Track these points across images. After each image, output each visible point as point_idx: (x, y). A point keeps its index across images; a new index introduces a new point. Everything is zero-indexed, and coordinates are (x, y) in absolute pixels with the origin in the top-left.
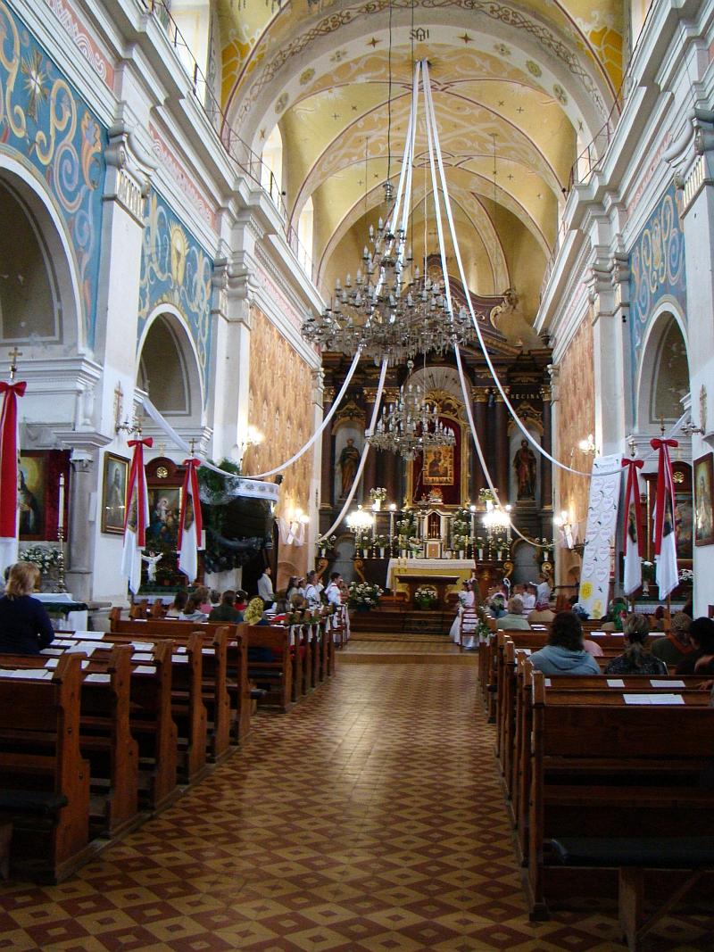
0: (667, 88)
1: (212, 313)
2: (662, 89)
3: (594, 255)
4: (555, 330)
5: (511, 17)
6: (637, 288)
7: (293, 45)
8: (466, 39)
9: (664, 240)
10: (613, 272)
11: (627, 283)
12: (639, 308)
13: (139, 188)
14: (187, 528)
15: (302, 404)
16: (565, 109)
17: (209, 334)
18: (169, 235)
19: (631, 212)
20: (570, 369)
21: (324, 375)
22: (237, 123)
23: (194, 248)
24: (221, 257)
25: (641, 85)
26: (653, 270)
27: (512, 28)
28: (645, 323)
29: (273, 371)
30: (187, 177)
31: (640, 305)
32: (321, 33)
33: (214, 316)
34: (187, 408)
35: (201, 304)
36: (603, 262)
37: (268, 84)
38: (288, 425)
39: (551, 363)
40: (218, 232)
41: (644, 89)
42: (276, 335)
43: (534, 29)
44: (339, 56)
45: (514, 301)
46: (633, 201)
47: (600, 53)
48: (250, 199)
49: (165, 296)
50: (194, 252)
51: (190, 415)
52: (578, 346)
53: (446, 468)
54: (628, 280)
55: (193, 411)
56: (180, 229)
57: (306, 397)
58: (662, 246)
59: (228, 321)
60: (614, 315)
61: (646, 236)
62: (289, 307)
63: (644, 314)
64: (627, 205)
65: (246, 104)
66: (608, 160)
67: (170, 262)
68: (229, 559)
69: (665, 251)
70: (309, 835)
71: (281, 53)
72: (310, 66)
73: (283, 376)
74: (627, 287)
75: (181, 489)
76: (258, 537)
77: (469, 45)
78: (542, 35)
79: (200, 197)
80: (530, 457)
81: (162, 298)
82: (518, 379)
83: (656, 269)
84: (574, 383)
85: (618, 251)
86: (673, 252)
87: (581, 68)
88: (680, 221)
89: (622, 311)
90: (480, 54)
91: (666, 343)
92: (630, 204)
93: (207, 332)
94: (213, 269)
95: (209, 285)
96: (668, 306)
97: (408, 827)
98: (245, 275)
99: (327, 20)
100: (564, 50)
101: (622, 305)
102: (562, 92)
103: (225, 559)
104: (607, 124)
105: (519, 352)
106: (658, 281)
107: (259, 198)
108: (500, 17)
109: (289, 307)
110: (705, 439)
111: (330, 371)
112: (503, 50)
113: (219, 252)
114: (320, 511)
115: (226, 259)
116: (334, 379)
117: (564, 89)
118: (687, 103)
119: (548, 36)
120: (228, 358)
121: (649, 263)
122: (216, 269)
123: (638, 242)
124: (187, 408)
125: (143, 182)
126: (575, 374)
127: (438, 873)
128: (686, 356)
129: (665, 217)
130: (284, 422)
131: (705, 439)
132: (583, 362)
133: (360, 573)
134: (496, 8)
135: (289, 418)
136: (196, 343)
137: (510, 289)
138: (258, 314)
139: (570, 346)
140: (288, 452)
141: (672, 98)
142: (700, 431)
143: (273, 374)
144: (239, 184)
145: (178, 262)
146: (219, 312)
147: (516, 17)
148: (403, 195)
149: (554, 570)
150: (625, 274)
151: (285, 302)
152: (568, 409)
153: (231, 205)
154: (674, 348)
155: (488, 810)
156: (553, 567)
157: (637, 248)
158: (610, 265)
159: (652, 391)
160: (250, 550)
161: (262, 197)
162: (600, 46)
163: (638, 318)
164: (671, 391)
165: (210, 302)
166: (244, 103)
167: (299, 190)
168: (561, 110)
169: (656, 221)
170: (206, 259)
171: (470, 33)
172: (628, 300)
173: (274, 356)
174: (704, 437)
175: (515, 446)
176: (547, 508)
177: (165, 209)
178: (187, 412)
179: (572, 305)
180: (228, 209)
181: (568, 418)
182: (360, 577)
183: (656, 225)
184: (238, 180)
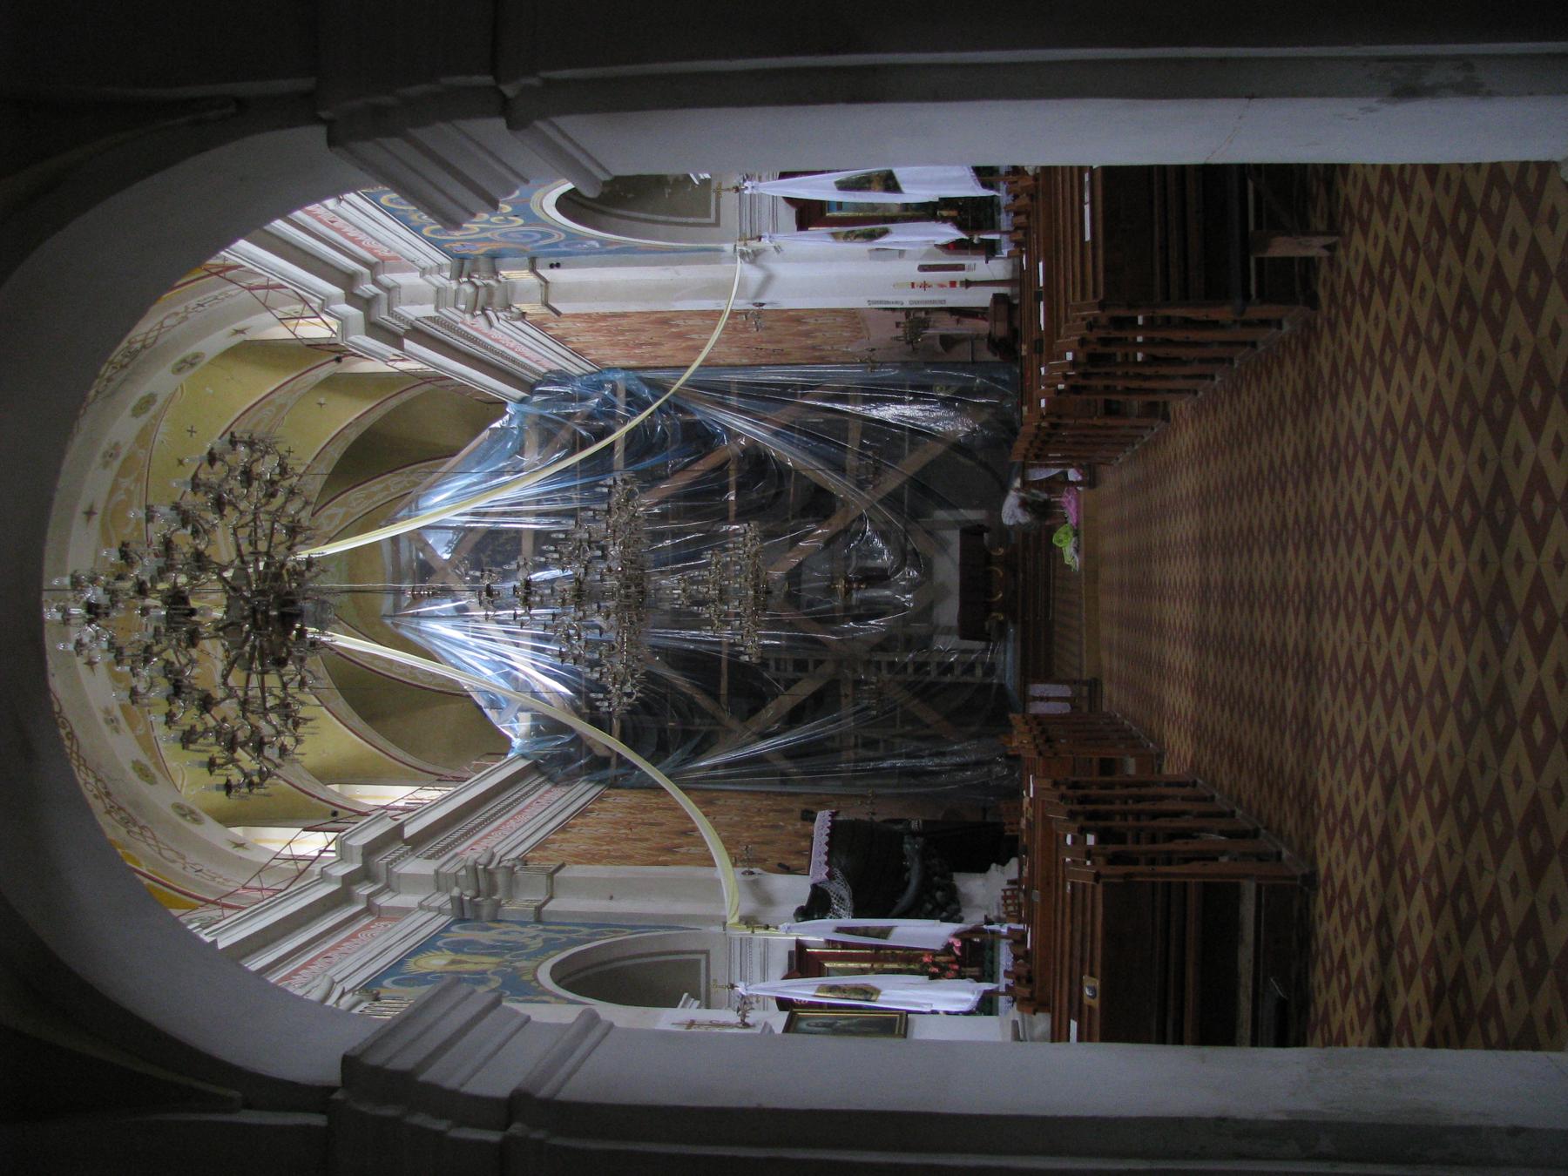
1: (539, 920)
3: (448, 312)
7: (95, 792)
8: (90, 513)
10: (478, 283)
11: (497, 262)
13: (365, 1004)
16: (209, 356)
18: (429, 974)
19: (385, 252)
22: (223, 884)
23: (439, 943)
24: (449, 906)
28: (565, 232)
30: (327, 951)
33: (545, 918)
35: (531, 936)
36: (462, 298)
37: (157, 834)
40: (406, 911)
42: (562, 836)
44: (111, 721)
46: (370, 250)
48: (352, 862)
49: (525, 978)
51: (707, 953)
52: (582, 339)
54: (494, 257)
55: (700, 948)
56: (413, 960)
59: (551, 898)
60: (546, 282)
64: (376, 260)
66: (307, 289)
67: (466, 972)
68: (939, 888)
71: (108, 812)
72: (128, 767)
73: (629, 826)
74: (508, 260)
77: (99, 509)
79: (354, 936)
81: (529, 982)
84: (640, 345)
85: (448, 274)
87: (151, 330)
89: (543, 268)
90: (113, 491)
92: (375, 255)
94: (468, 920)
98: (475, 870)
100: (120, 357)
101: (533, 270)
102: (184, 361)
103: (939, 894)
104: (250, 289)
106: (505, 215)
109: (513, 818)
112: (111, 455)
113: (440, 911)
117: (179, 358)
120: (611, 898)
122: (467, 916)
125: (356, 998)
132: (609, 331)
136: (589, 942)
138: (553, 842)
143: (627, 839)
144: (330, 876)
145: (466, 962)
146: (539, 909)
148: (1064, 227)
150: (483, 265)
153: (364, 890)
158: (468, 289)
161: (349, 842)
163: (555, 245)
165: (524, 924)
166: (190, 873)
167: (315, 800)
168: (210, 363)
170: (454, 928)
171: (82, 506)
172: (526, 260)
177: (392, 976)
178: (703, 957)
179: (513, 349)
180: (369, 896)
184: (324, 877)
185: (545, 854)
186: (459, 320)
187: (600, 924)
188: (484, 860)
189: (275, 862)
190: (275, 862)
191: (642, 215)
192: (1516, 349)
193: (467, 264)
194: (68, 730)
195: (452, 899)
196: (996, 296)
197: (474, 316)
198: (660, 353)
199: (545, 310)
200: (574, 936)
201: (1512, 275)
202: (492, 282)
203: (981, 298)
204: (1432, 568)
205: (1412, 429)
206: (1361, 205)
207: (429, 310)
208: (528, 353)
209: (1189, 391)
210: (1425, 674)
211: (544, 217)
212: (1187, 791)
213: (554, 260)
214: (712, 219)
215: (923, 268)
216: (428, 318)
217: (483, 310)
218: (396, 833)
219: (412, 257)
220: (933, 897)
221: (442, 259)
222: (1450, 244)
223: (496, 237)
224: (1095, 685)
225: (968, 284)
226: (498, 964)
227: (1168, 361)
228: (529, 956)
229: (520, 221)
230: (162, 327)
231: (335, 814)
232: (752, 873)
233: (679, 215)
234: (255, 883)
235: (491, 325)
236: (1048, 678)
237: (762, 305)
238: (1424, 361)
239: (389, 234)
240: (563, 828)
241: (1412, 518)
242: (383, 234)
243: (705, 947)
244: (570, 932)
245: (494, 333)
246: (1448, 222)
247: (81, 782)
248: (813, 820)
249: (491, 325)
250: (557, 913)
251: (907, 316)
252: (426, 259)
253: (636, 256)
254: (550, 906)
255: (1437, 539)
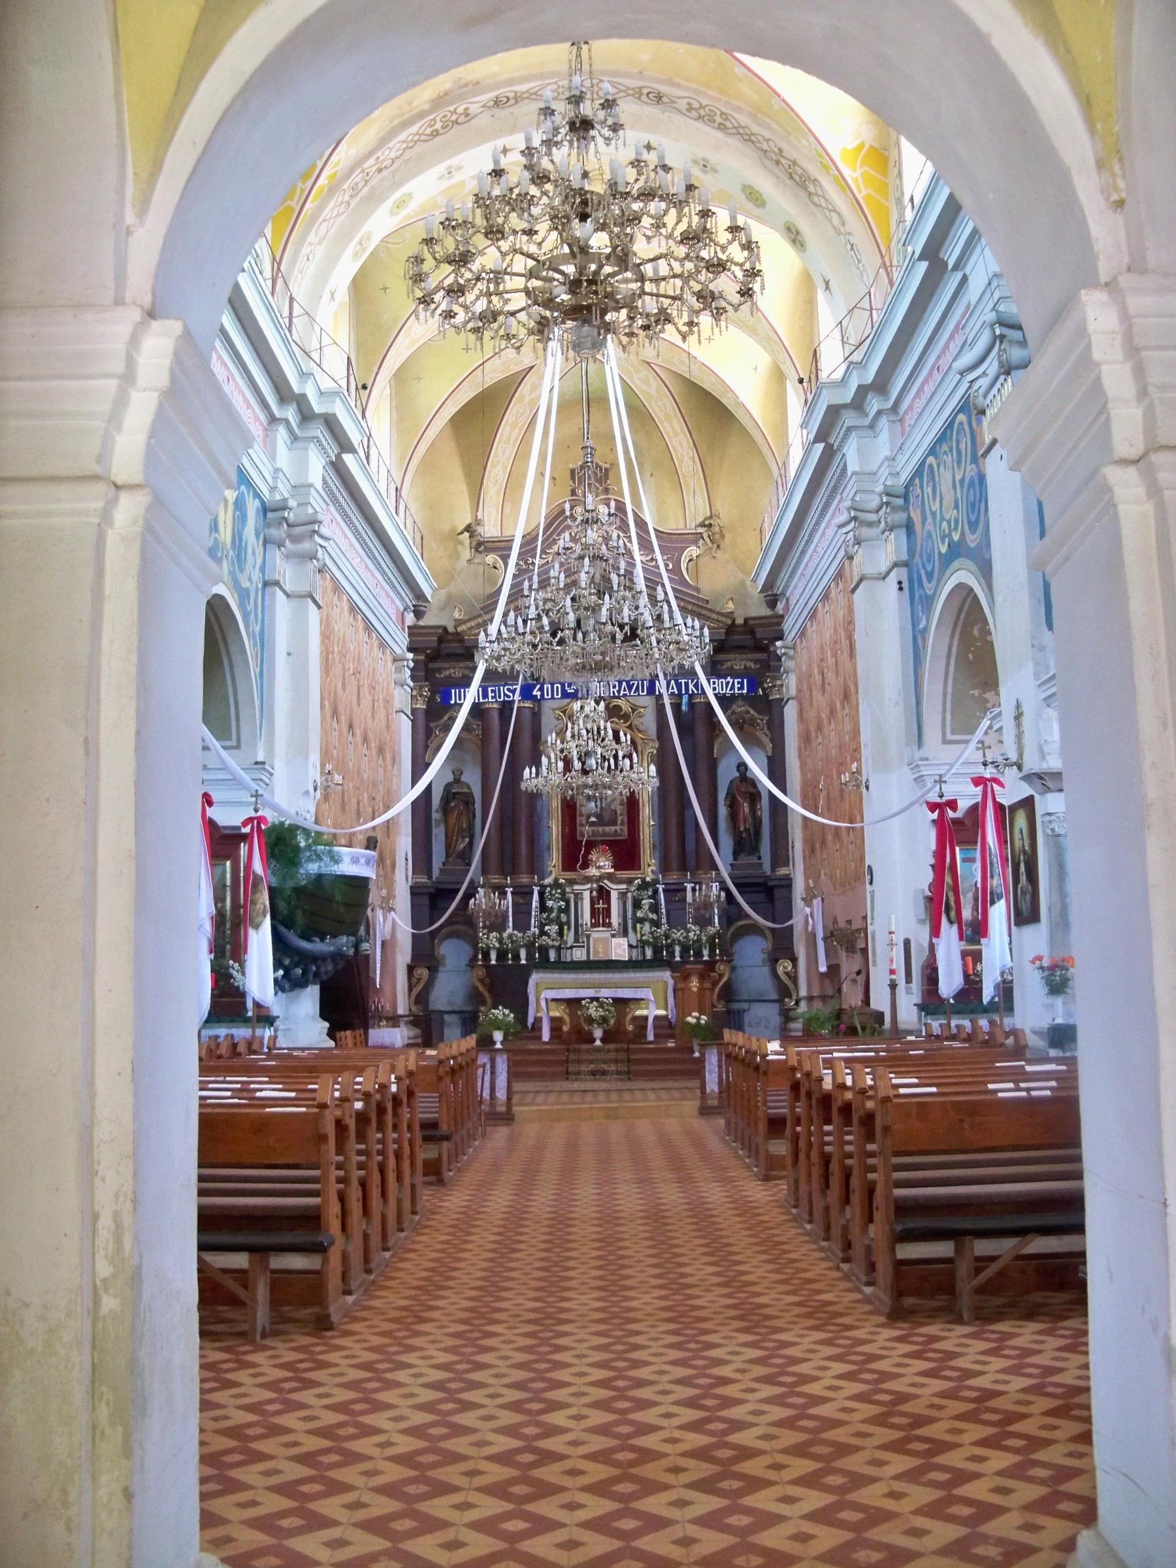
0: (956, 268)
1: (266, 584)
2: (950, 266)
4: (787, 586)
5: (718, 119)
6: (919, 542)
9: (958, 477)
12: (923, 572)
14: (257, 927)
15: (381, 714)
17: (263, 619)
19: (909, 421)
20: (815, 652)
21: (412, 664)
23: (243, 488)
24: (278, 497)
25: (921, 258)
26: (942, 519)
27: (719, 135)
29: (343, 665)
31: (924, 567)
32: (423, 138)
33: (268, 590)
34: (234, 736)
36: (865, 497)
37: (342, 218)
38: (365, 751)
39: (781, 638)
40: (272, 457)
41: (924, 265)
43: (753, 138)
45: (717, 536)
46: (910, 408)
47: (855, 180)
50: (243, 493)
51: (238, 747)
53: (615, 811)
54: (909, 527)
57: (387, 702)
58: (954, 487)
59: (288, 596)
61: (931, 466)
62: (362, 560)
63: (930, 580)
65: (308, 251)
68: (305, 972)
69: (959, 495)
70: (379, 1450)
71: (363, 171)
75: (228, 863)
76: (348, 935)
78: (765, 147)
80: (752, 790)
82: (729, 664)
83: (947, 517)
85: (889, 483)
86: (971, 498)
88: (981, 460)
89: (897, 574)
91: (964, 626)
92: (906, 412)
93: (260, 616)
94: (265, 515)
95: (261, 542)
96: (963, 575)
97: (574, 1395)
99: (434, 119)
105: (729, 622)
106: (950, 535)
107: (334, 402)
108: (700, 118)
109: (362, 560)
110: (1022, 778)
111: (422, 657)
113: (273, 489)
114: (411, 888)
115: (285, 500)
116: (427, 670)
118: (984, 302)
119: (776, 150)
120: (289, 654)
121: (936, 507)
122: (270, 515)
123: (918, 472)
124: (234, 736)
126: (822, 660)
127: (633, 1464)
128: (991, 644)
129: (958, 442)
130: (360, 746)
131: (1022, 778)
132: (822, 660)
133: (481, 988)
134: (696, 105)
135: (365, 739)
137: (711, 517)
139: (813, 615)
140: (366, 795)
141: (965, 279)
142: (1015, 764)
143: (344, 670)
146: (277, 583)
147: (726, 119)
149: (796, 972)
151: (357, 552)
152: (811, 714)
153: (291, 414)
154: (976, 632)
155: (696, 1381)
156: (795, 966)
157: (917, 481)
158: (874, 502)
159: (945, 694)
160: (337, 956)
162: (855, 171)
164: (973, 695)
166: (306, 250)
167: (375, 370)
169: (945, 448)
170: (257, 502)
173: (344, 642)
174: (1021, 775)
175: (726, 774)
176: (783, 871)
179: (815, 551)
180: (287, 421)
181: (812, 728)
182: (482, 995)
183: (945, 453)
184: (304, 375)
185: (329, 591)
186: (844, 495)
187: (264, 642)
188: (324, 530)
189: (317, 328)
190: (317, 328)
191: (952, 668)
192: (895, 1495)
193: (900, 501)
194: (441, 131)
195: (285, 500)
196: (882, 1014)
197: (849, 509)
198: (814, 693)
199: (856, 579)
200: (252, 616)
201: (968, 1490)
202: (883, 525)
203: (880, 1001)
204: (664, 1422)
205: (800, 1401)
206: (1014, 1348)
207: (853, 465)
208: (812, 565)
209: (797, 1200)
210: (557, 1418)
211: (948, 573)
212: (407, 1204)
213: (905, 585)
214: (949, 737)
215: (907, 943)
216: (845, 466)
217: (855, 518)
218: (345, 445)
219: (905, 448)
220: (297, 965)
221: (904, 477)
222: (989, 1431)
223: (927, 527)
224: (507, 1118)
225: (893, 986)
226: (224, 543)
227: (826, 1177)
228: (232, 573)
229: (944, 549)
230: (830, 211)
231: (364, 387)
232: (315, 790)
233: (953, 703)
234: (297, 310)
235: (841, 526)
236: (513, 1076)
237: (867, 788)
238: (869, 1410)
239: (928, 423)
240: (354, 609)
241: (709, 1402)
242: (928, 419)
243: (243, 744)
244: (256, 615)
245: (830, 533)
246: (1011, 1428)
247: (391, 145)
248: (367, 848)
249: (841, 526)
250: (273, 603)
251: (858, 931)
252: (904, 461)
253: (911, 665)
254: (279, 594)
255: (694, 1426)
